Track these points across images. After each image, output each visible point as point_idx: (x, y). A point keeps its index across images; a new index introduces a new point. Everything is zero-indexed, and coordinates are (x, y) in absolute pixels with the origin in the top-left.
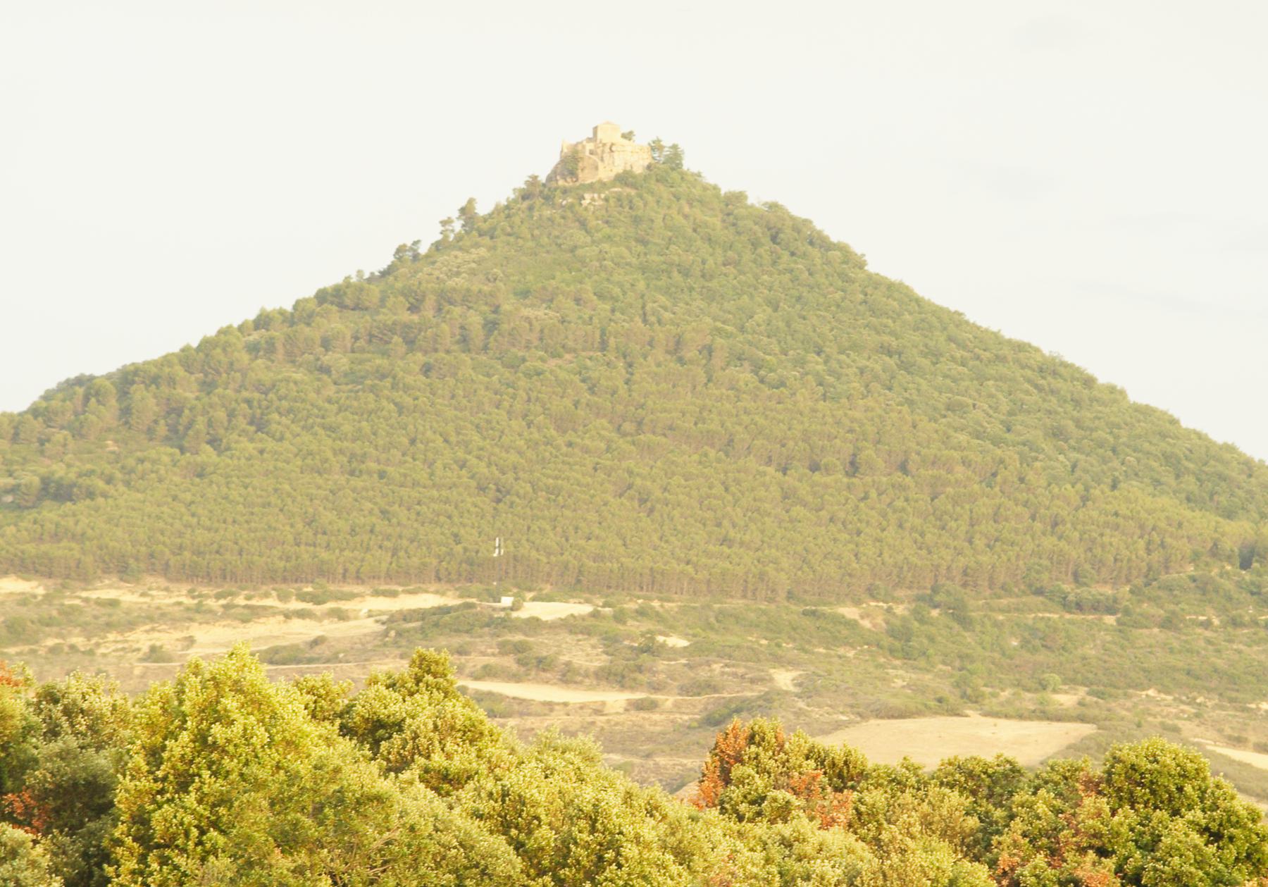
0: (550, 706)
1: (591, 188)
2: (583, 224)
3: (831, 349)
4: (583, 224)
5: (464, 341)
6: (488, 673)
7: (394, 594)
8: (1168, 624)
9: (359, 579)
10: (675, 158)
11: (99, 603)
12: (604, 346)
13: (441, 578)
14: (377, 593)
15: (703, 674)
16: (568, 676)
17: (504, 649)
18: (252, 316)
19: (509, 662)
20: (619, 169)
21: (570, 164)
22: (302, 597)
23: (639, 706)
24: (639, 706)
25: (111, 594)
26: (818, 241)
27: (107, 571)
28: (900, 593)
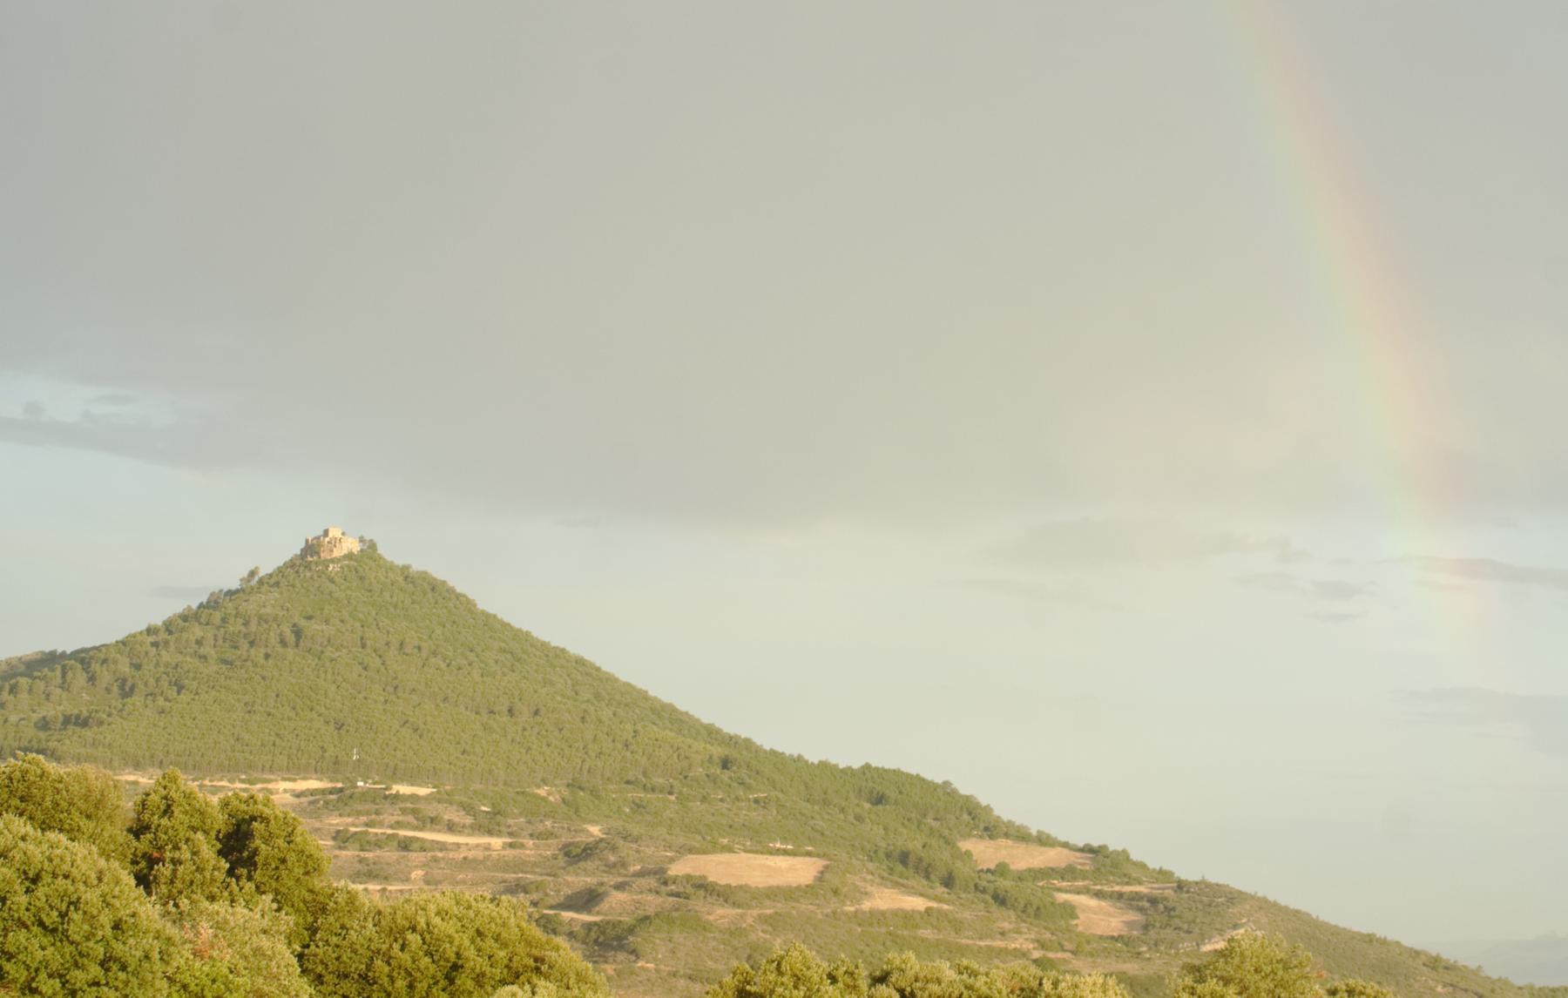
0: (458, 845)
1: (332, 561)
2: (332, 581)
3: (478, 649)
4: (332, 581)
5: (283, 643)
6: (399, 825)
7: (294, 780)
8: (704, 799)
9: (271, 770)
10: (373, 545)
11: (128, 782)
12: (364, 646)
13: (318, 772)
14: (284, 779)
15: (541, 828)
16: (451, 828)
17: (404, 811)
18: (144, 627)
19: (410, 819)
20: (345, 551)
21: (311, 549)
22: (242, 781)
23: (511, 845)
24: (511, 845)
25: (132, 778)
26: (451, 591)
27: (126, 764)
28: (557, 782)
